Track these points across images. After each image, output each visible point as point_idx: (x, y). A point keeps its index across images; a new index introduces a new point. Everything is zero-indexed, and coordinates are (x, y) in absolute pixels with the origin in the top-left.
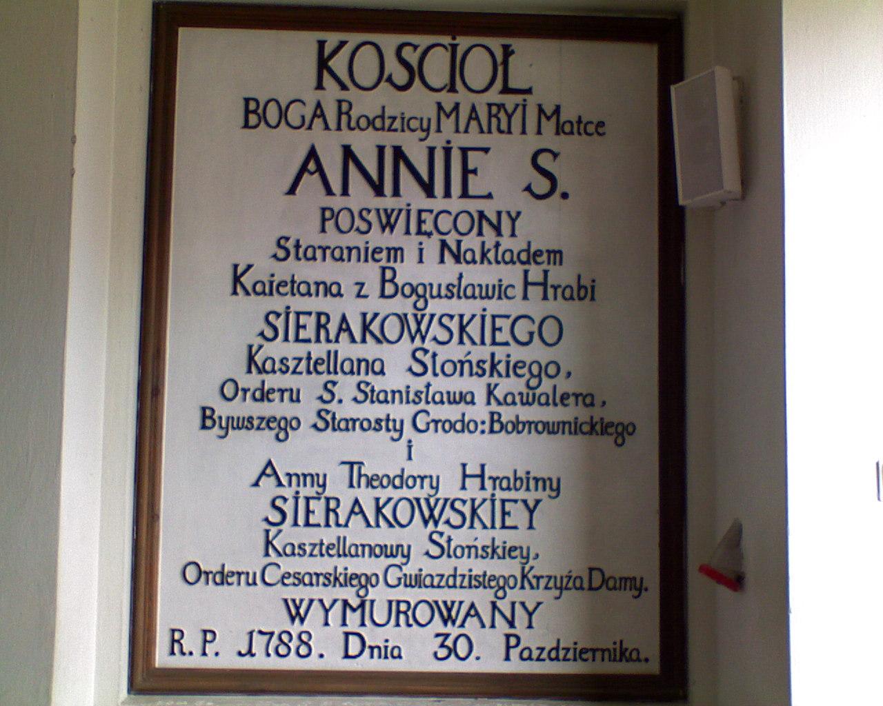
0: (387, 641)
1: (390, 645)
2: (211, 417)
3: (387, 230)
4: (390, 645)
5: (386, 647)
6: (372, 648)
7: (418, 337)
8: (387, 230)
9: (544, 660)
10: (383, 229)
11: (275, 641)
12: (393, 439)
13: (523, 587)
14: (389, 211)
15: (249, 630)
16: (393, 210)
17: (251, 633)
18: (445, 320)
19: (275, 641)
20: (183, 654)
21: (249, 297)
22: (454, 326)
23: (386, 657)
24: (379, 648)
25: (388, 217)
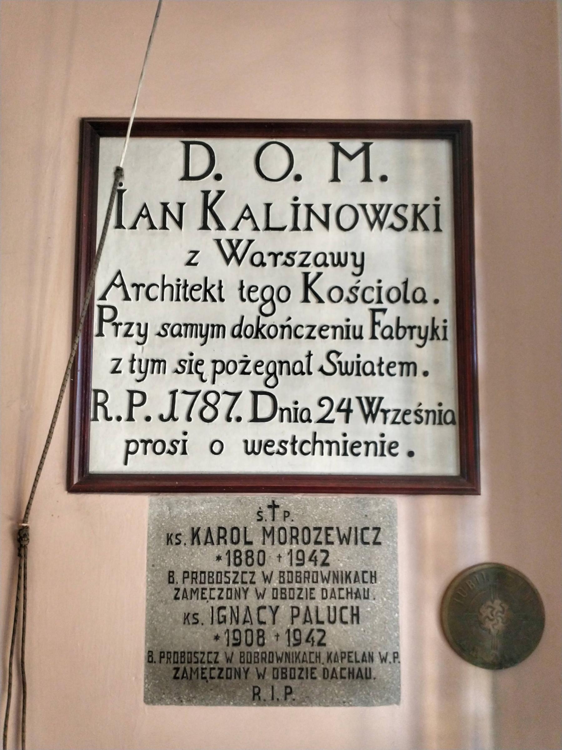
0: (296, 403)
1: (300, 406)
2: (284, 593)
3: (370, 419)
4: (300, 406)
5: (296, 409)
6: (282, 410)
7: (377, 224)
8: (370, 419)
9: (399, 423)
10: (372, 226)
11: (199, 403)
12: (338, 354)
13: (415, 229)
14: (378, 208)
15: (172, 389)
16: (374, 399)
17: (173, 393)
18: (400, 211)
19: (199, 403)
20: (109, 419)
21: (264, 340)
22: (409, 214)
23: (296, 421)
24: (288, 409)
25: (377, 213)
